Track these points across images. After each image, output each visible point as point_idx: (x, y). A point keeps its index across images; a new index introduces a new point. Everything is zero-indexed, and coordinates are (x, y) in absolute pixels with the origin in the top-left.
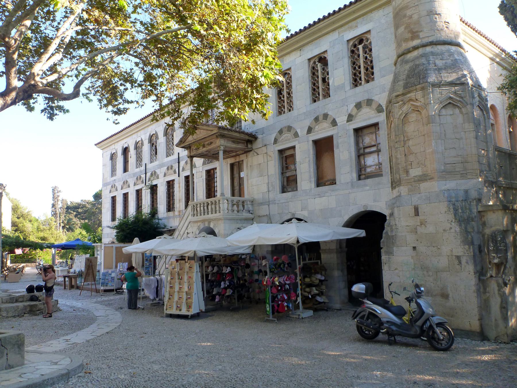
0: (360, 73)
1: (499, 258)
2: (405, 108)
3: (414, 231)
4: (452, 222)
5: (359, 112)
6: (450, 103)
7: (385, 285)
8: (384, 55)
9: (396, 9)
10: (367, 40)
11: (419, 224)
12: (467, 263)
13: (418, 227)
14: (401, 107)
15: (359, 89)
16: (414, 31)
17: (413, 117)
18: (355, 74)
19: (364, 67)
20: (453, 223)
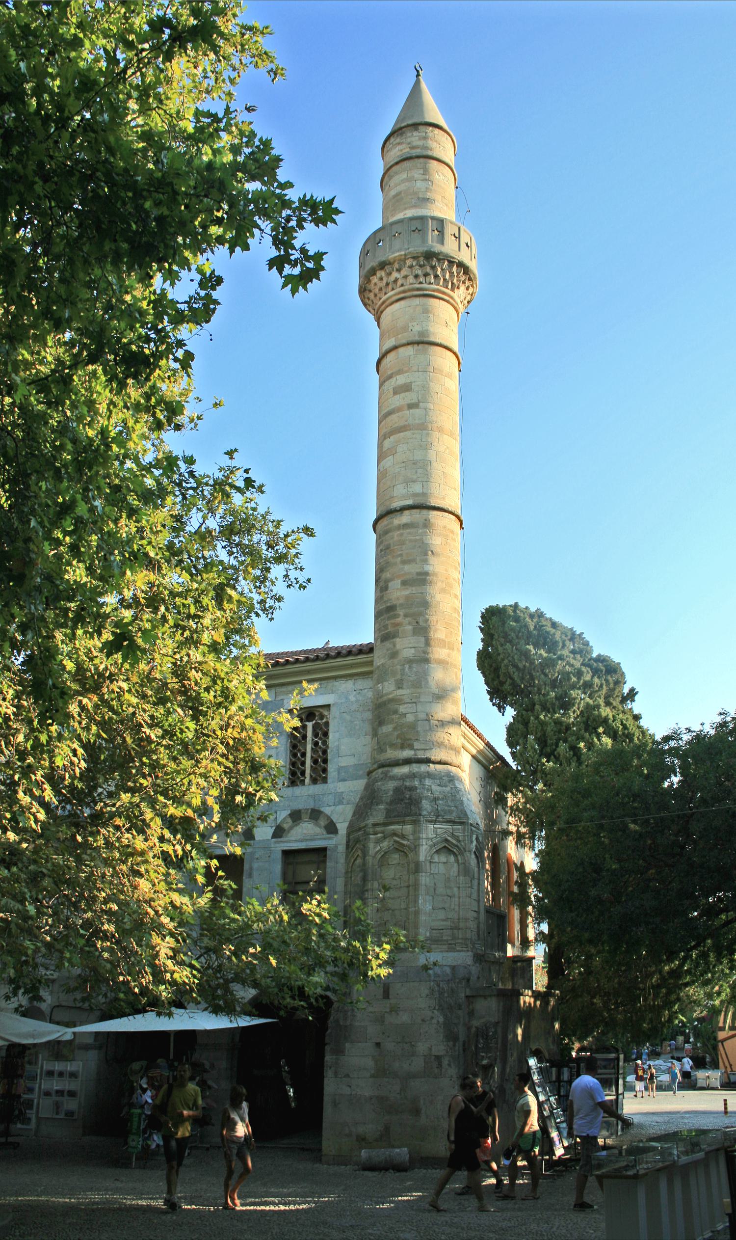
0: (303, 764)
1: (489, 1058)
2: (385, 844)
3: (380, 1020)
4: (434, 1009)
5: (297, 825)
6: (445, 847)
7: (326, 1099)
8: (348, 747)
9: (382, 696)
10: (322, 717)
11: (388, 1010)
12: (449, 1065)
13: (386, 1015)
14: (378, 841)
15: (298, 790)
16: (408, 737)
17: (395, 858)
18: (293, 764)
19: (312, 757)
20: (435, 1012)
